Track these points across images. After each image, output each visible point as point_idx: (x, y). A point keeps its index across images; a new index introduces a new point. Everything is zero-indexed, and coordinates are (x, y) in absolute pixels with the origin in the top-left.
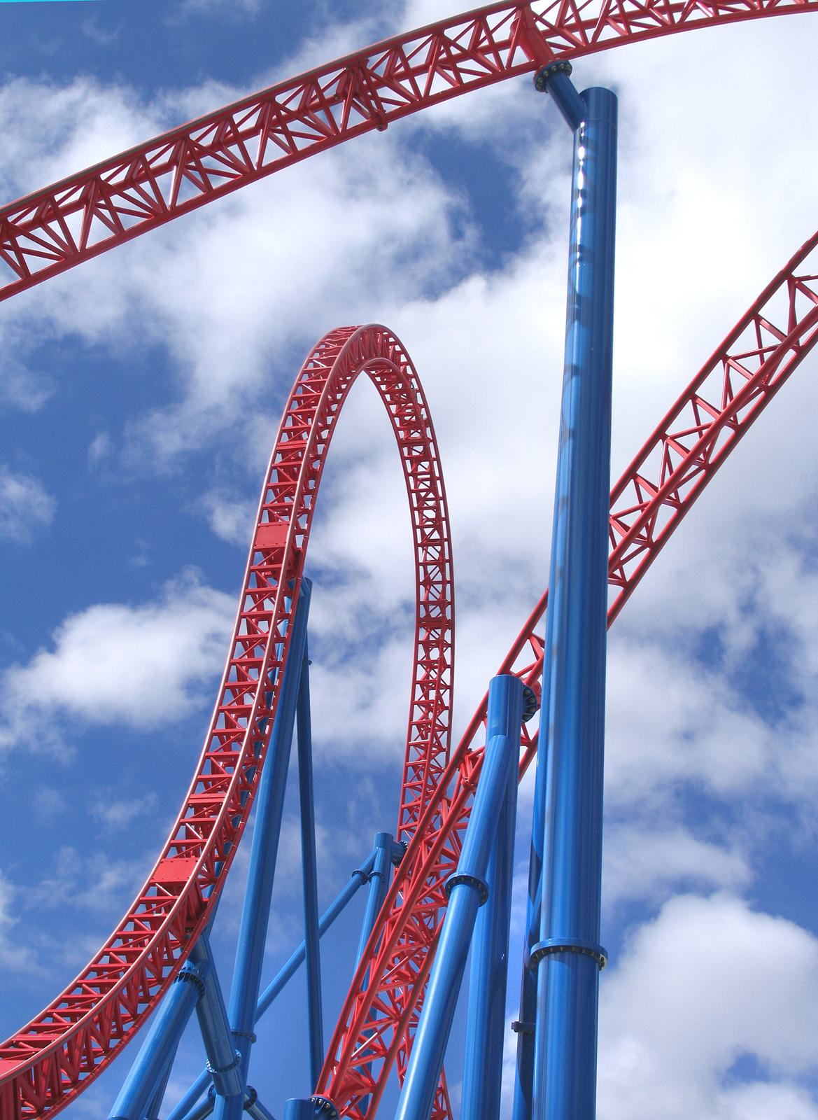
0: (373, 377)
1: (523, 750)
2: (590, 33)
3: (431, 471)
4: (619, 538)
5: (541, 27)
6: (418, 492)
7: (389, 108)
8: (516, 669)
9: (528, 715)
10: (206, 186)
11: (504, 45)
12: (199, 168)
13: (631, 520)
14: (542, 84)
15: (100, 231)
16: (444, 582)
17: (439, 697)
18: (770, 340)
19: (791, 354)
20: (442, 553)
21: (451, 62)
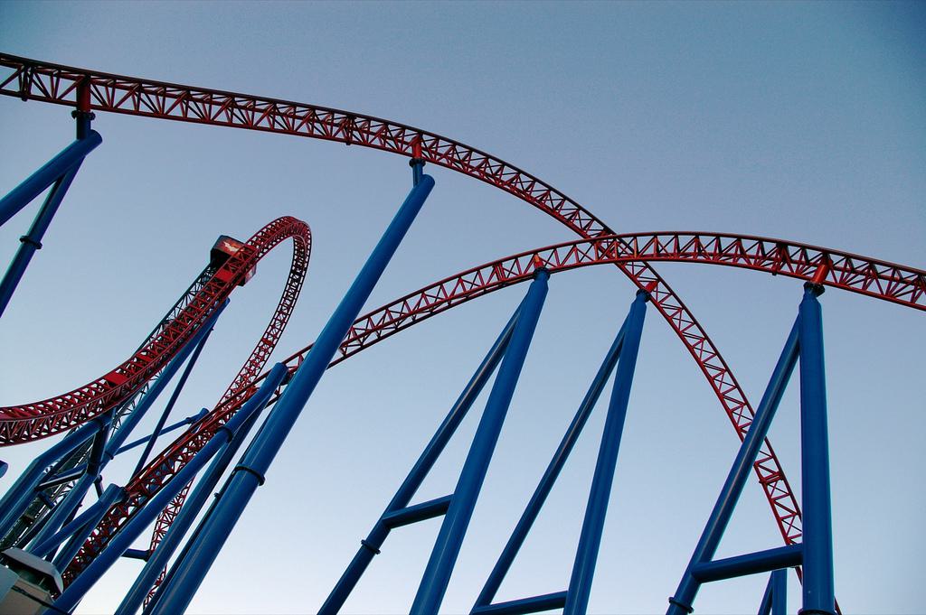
0: (294, 241)
1: (274, 396)
2: (438, 157)
3: (297, 287)
4: (352, 336)
5: (423, 145)
6: (288, 291)
7: (354, 139)
8: (288, 365)
9: (283, 384)
10: (185, 113)
11: (406, 143)
12: (274, 119)
13: (359, 333)
14: (412, 163)
15: (177, 112)
16: (279, 330)
17: (255, 370)
18: (442, 295)
19: (446, 304)
20: (284, 319)
21: (385, 138)
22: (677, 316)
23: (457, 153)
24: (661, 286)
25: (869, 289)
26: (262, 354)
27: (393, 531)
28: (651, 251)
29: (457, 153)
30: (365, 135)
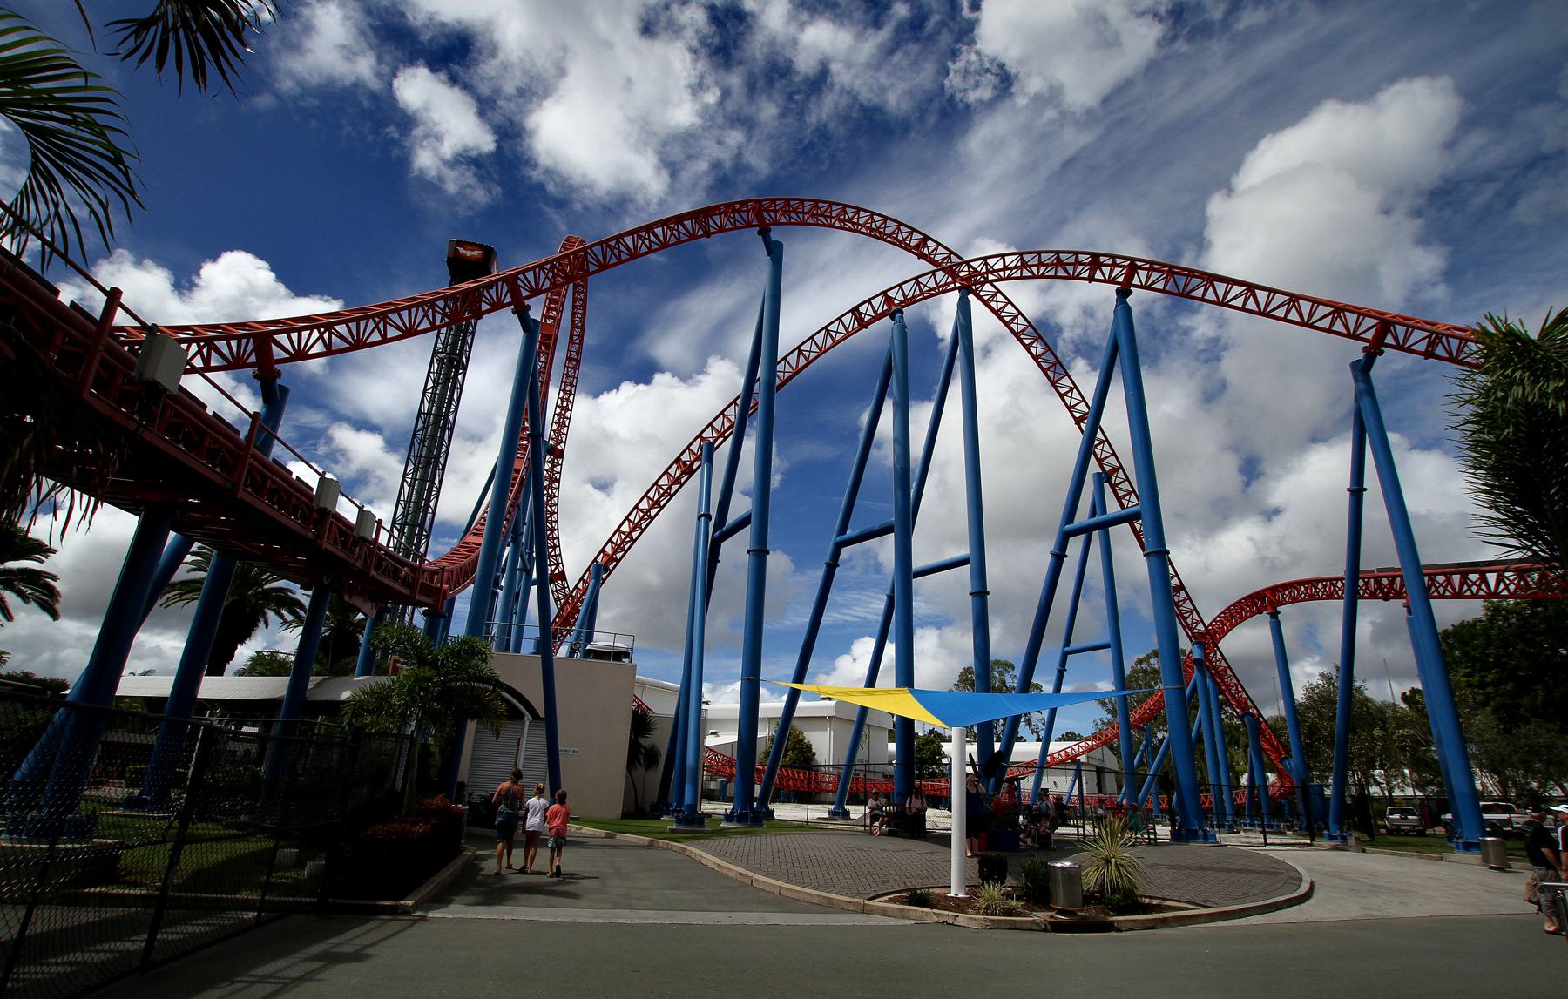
22: (807, 354)
23: (902, 233)
24: (891, 294)
25: (213, 364)
26: (568, 388)
27: (723, 544)
28: (984, 270)
29: (875, 222)
30: (828, 220)
